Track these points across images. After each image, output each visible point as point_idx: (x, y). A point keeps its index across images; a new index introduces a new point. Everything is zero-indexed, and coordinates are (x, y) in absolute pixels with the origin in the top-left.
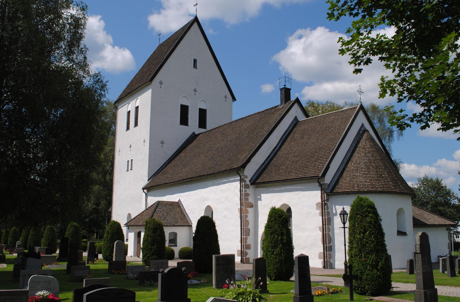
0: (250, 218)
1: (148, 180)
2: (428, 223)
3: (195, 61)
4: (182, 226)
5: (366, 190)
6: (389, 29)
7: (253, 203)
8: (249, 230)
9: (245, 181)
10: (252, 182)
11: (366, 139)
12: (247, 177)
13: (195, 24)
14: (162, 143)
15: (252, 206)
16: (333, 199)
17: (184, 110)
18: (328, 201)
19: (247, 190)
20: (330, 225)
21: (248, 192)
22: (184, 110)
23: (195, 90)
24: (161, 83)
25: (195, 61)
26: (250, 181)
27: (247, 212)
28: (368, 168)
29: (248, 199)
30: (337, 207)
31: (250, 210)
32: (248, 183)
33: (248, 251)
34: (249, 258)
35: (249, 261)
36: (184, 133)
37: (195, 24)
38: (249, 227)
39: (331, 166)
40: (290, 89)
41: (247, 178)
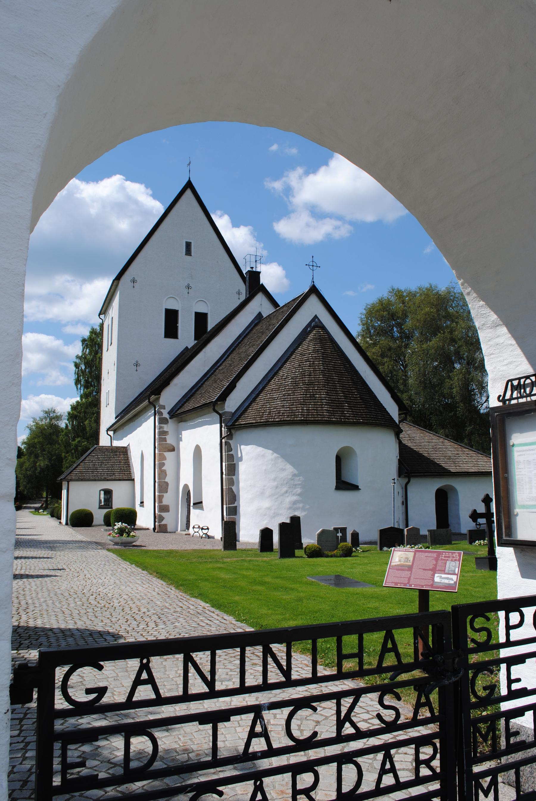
0: (169, 467)
1: (116, 418)
2: (453, 469)
3: (188, 245)
4: (120, 480)
5: (277, 420)
6: (98, 185)
7: (174, 444)
8: (167, 484)
9: (161, 414)
10: (172, 414)
11: (311, 340)
12: (164, 407)
13: (189, 192)
14: (137, 365)
15: (173, 450)
16: (239, 435)
17: (171, 317)
18: (231, 439)
19: (165, 426)
20: (234, 475)
21: (165, 429)
22: (171, 317)
23: (188, 287)
24: (134, 281)
25: (188, 245)
26: (169, 413)
27: (165, 458)
28: (295, 384)
29: (165, 440)
30: (242, 447)
31: (169, 455)
32: (166, 415)
33: (164, 514)
34: (165, 526)
35: (166, 529)
36: (173, 348)
37: (189, 192)
38: (166, 480)
39: (240, 385)
40: (260, 273)
41: (165, 409)
